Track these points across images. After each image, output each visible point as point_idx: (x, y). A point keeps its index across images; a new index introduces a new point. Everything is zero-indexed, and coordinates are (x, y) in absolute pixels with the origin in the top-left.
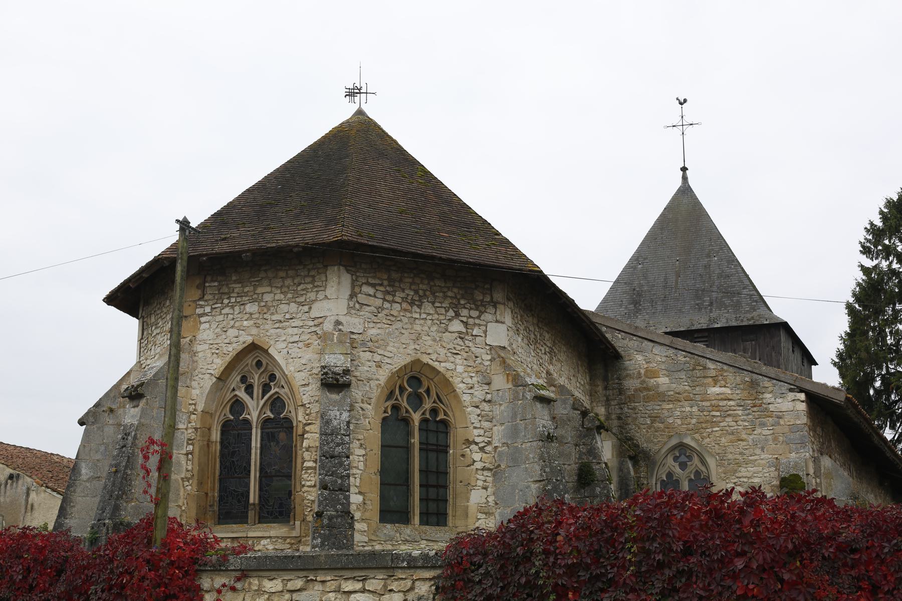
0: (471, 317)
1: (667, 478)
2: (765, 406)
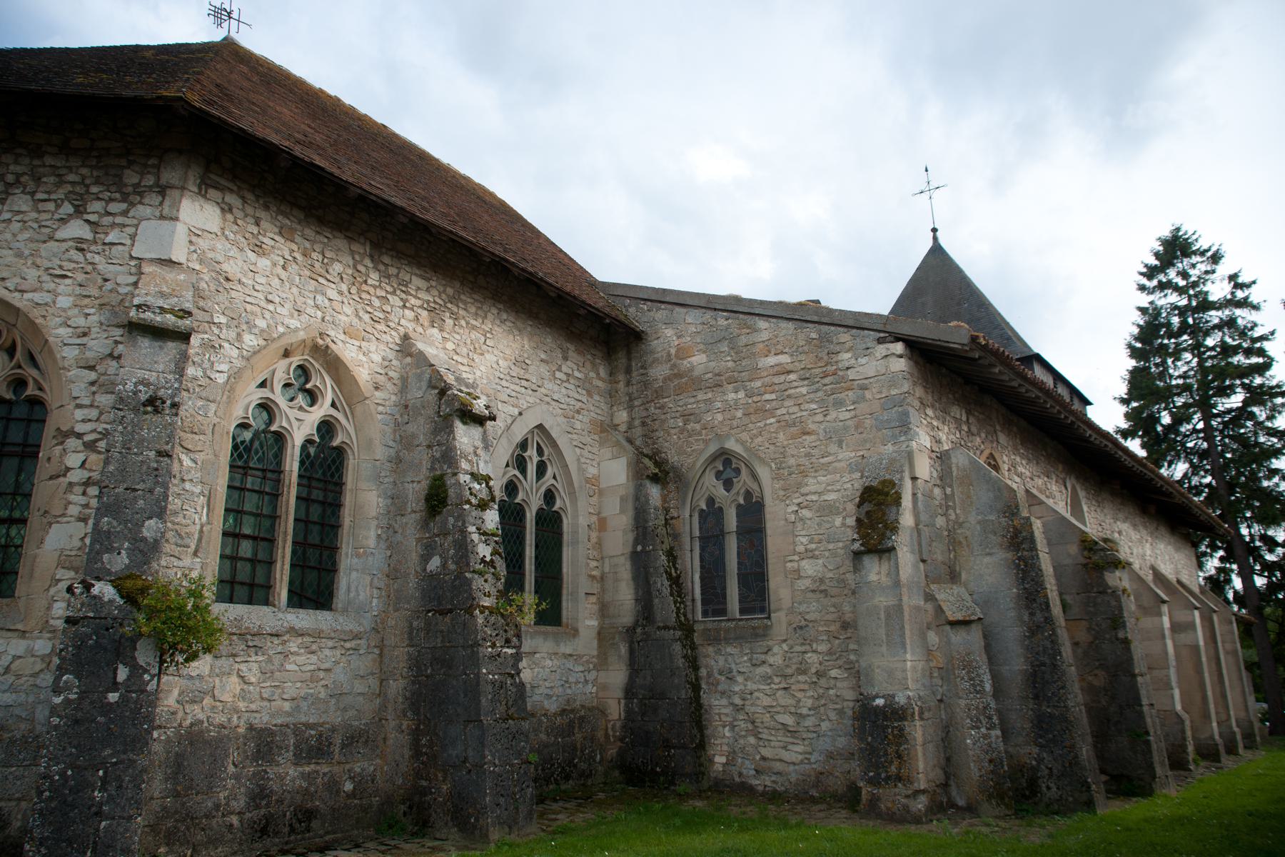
0: (109, 214)
1: (707, 506)
2: (841, 373)
